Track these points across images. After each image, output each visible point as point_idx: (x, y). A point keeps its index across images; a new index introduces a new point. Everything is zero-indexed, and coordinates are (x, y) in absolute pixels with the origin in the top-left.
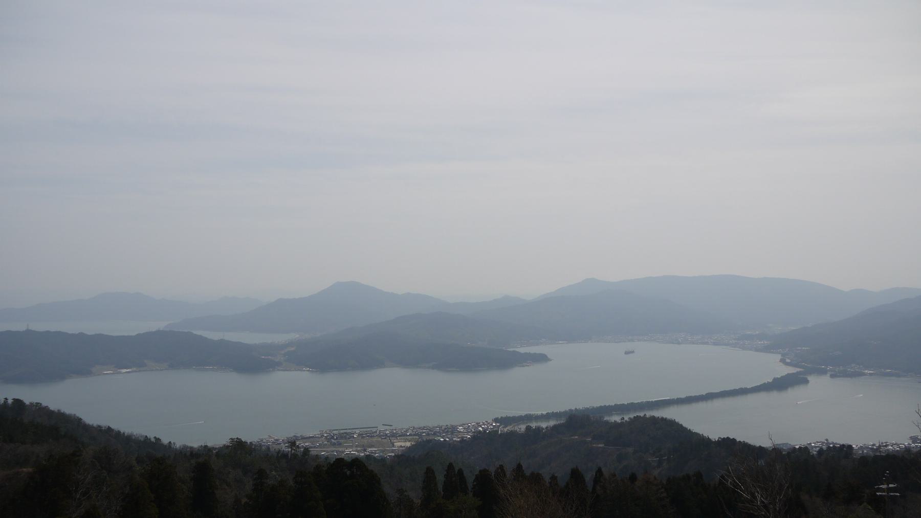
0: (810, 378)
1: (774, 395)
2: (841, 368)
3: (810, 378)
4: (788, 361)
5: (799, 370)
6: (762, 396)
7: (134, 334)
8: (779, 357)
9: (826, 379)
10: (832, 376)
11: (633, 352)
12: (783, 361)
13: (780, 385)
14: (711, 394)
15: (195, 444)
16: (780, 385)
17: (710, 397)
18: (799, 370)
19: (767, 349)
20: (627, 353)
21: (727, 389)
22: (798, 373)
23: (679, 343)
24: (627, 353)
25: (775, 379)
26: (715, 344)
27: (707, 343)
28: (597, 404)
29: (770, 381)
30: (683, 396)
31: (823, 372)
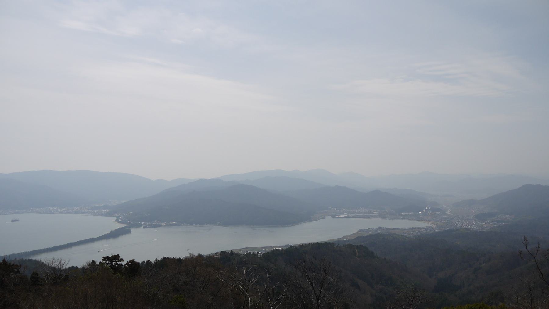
0: (132, 230)
1: (111, 241)
2: (150, 223)
3: (132, 230)
4: (120, 220)
5: (126, 225)
6: (104, 242)
7: (16, 253)
8: (115, 218)
9: (141, 229)
10: (144, 228)
11: (17, 220)
12: (117, 221)
13: (114, 235)
14: (93, 238)
15: (19, 252)
16: (114, 235)
17: (92, 240)
18: (126, 225)
19: (108, 214)
20: (13, 221)
21: (58, 245)
22: (127, 227)
23: (52, 213)
24: (13, 221)
25: (112, 232)
26: (76, 213)
27: (70, 212)
28: (23, 251)
29: (109, 233)
30: (51, 246)
31: (137, 226)
